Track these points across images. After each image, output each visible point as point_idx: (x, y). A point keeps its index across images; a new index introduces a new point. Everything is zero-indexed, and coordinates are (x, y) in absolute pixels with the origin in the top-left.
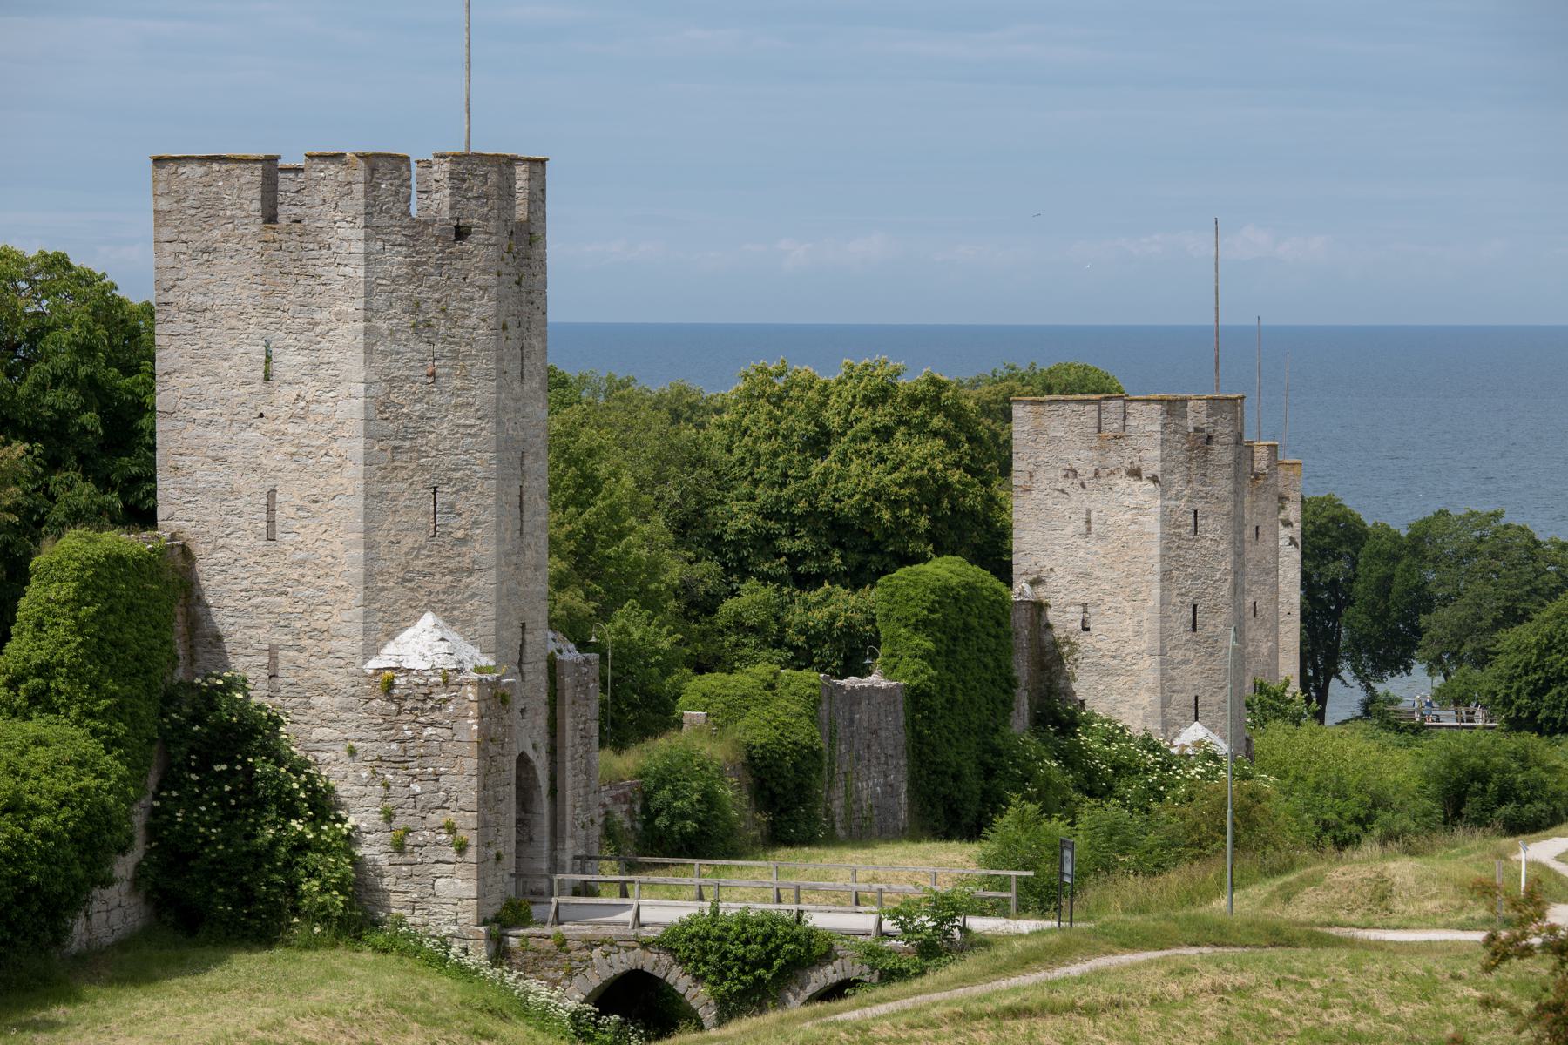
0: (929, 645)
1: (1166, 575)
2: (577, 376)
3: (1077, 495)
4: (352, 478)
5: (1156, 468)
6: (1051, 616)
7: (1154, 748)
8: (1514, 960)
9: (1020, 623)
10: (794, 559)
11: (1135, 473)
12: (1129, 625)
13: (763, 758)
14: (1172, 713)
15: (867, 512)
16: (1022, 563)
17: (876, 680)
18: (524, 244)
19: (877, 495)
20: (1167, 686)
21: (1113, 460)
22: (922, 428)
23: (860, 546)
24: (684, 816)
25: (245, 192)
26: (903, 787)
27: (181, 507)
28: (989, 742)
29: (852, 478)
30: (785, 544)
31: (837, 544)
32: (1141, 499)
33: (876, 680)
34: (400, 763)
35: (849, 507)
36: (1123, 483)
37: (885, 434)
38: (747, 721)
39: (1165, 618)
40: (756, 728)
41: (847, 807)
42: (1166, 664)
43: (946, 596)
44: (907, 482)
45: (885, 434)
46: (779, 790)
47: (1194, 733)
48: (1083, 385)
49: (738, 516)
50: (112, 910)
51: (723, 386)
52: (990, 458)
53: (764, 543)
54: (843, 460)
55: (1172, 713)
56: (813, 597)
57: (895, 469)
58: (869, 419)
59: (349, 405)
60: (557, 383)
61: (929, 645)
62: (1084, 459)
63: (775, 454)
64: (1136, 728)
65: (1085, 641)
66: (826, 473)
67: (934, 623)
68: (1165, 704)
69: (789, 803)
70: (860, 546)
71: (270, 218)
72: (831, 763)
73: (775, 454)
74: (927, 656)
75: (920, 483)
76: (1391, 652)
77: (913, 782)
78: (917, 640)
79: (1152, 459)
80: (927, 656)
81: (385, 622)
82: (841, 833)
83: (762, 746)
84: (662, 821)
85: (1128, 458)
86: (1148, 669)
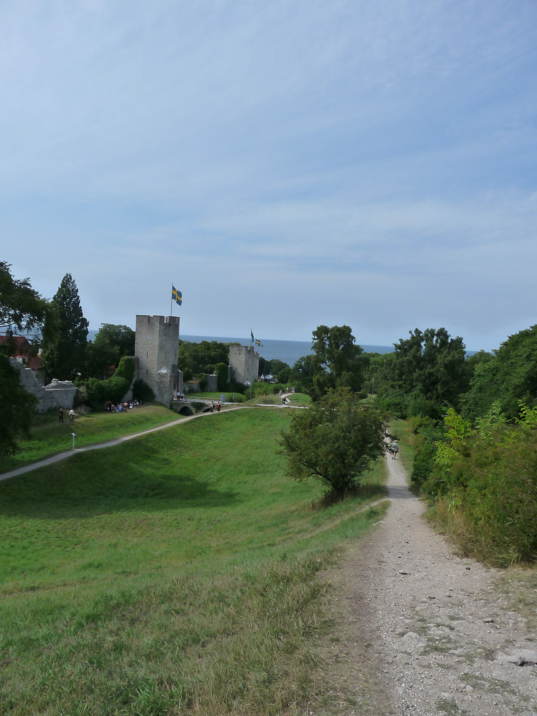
2: (305, 336)
4: (157, 351)
9: (229, 370)
16: (230, 363)
17: (214, 375)
18: (177, 326)
23: (213, 360)
25: (146, 320)
27: (137, 354)
28: (229, 384)
33: (214, 375)
34: (161, 383)
43: (221, 366)
45: (215, 348)
48: (238, 345)
50: (129, 394)
51: (199, 342)
52: (228, 351)
59: (157, 343)
60: (181, 343)
62: (237, 352)
69: (203, 387)
70: (213, 360)
71: (149, 322)
76: (267, 373)
81: (160, 368)
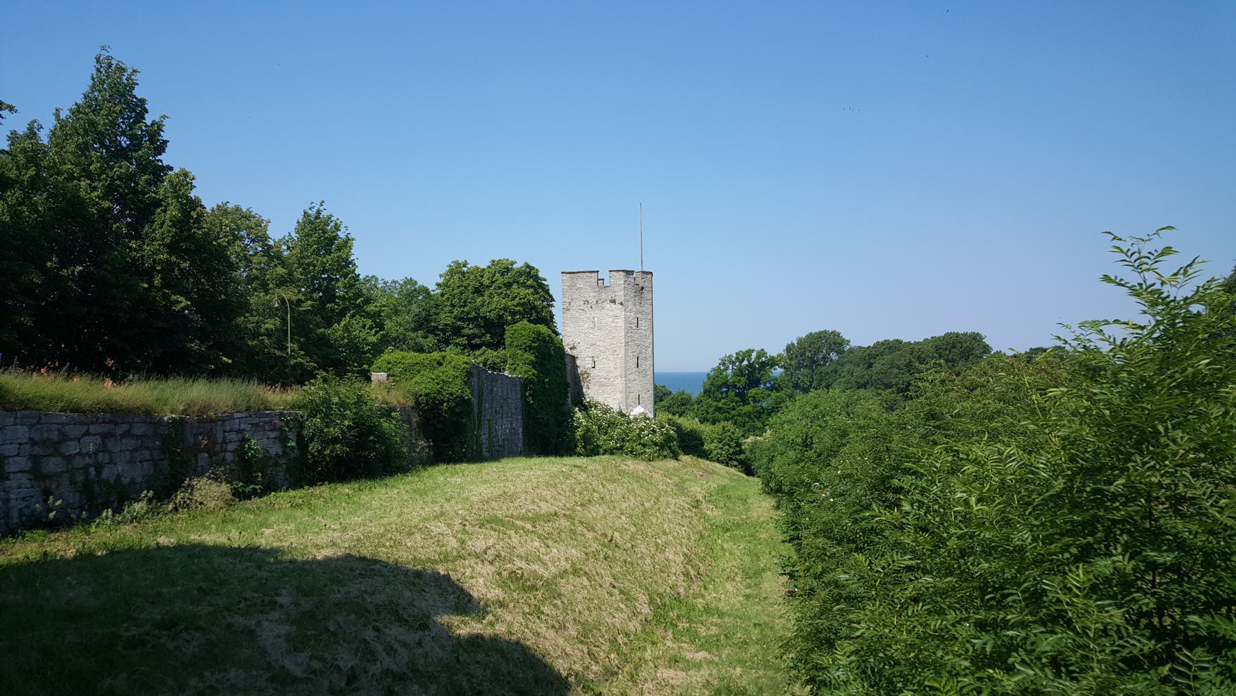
0: (532, 358)
1: (627, 343)
3: (589, 311)
5: (622, 299)
6: (578, 362)
7: (623, 415)
8: (755, 483)
9: (567, 360)
10: (470, 338)
11: (613, 302)
12: (611, 365)
13: (427, 404)
14: (630, 401)
15: (501, 317)
19: (505, 309)
20: (627, 391)
21: (604, 296)
22: (524, 285)
24: (335, 440)
26: (520, 430)
29: (493, 304)
30: (466, 331)
31: (488, 332)
32: (616, 312)
35: (492, 315)
36: (608, 305)
37: (508, 285)
38: (417, 379)
39: (626, 361)
40: (423, 383)
41: (489, 439)
42: (627, 381)
44: (518, 305)
45: (508, 285)
46: (439, 426)
47: (638, 410)
49: (445, 319)
53: (457, 331)
54: (491, 296)
55: (630, 401)
56: (478, 353)
57: (513, 299)
58: (501, 280)
61: (532, 358)
62: (591, 296)
63: (461, 293)
64: (616, 408)
65: (593, 373)
66: (484, 302)
67: (534, 348)
68: (627, 398)
72: (480, 412)
73: (461, 293)
74: (532, 364)
75: (522, 305)
77: (525, 428)
78: (526, 356)
79: (620, 295)
80: (532, 364)
82: (487, 454)
83: (426, 395)
84: (314, 447)
85: (610, 295)
86: (619, 383)
